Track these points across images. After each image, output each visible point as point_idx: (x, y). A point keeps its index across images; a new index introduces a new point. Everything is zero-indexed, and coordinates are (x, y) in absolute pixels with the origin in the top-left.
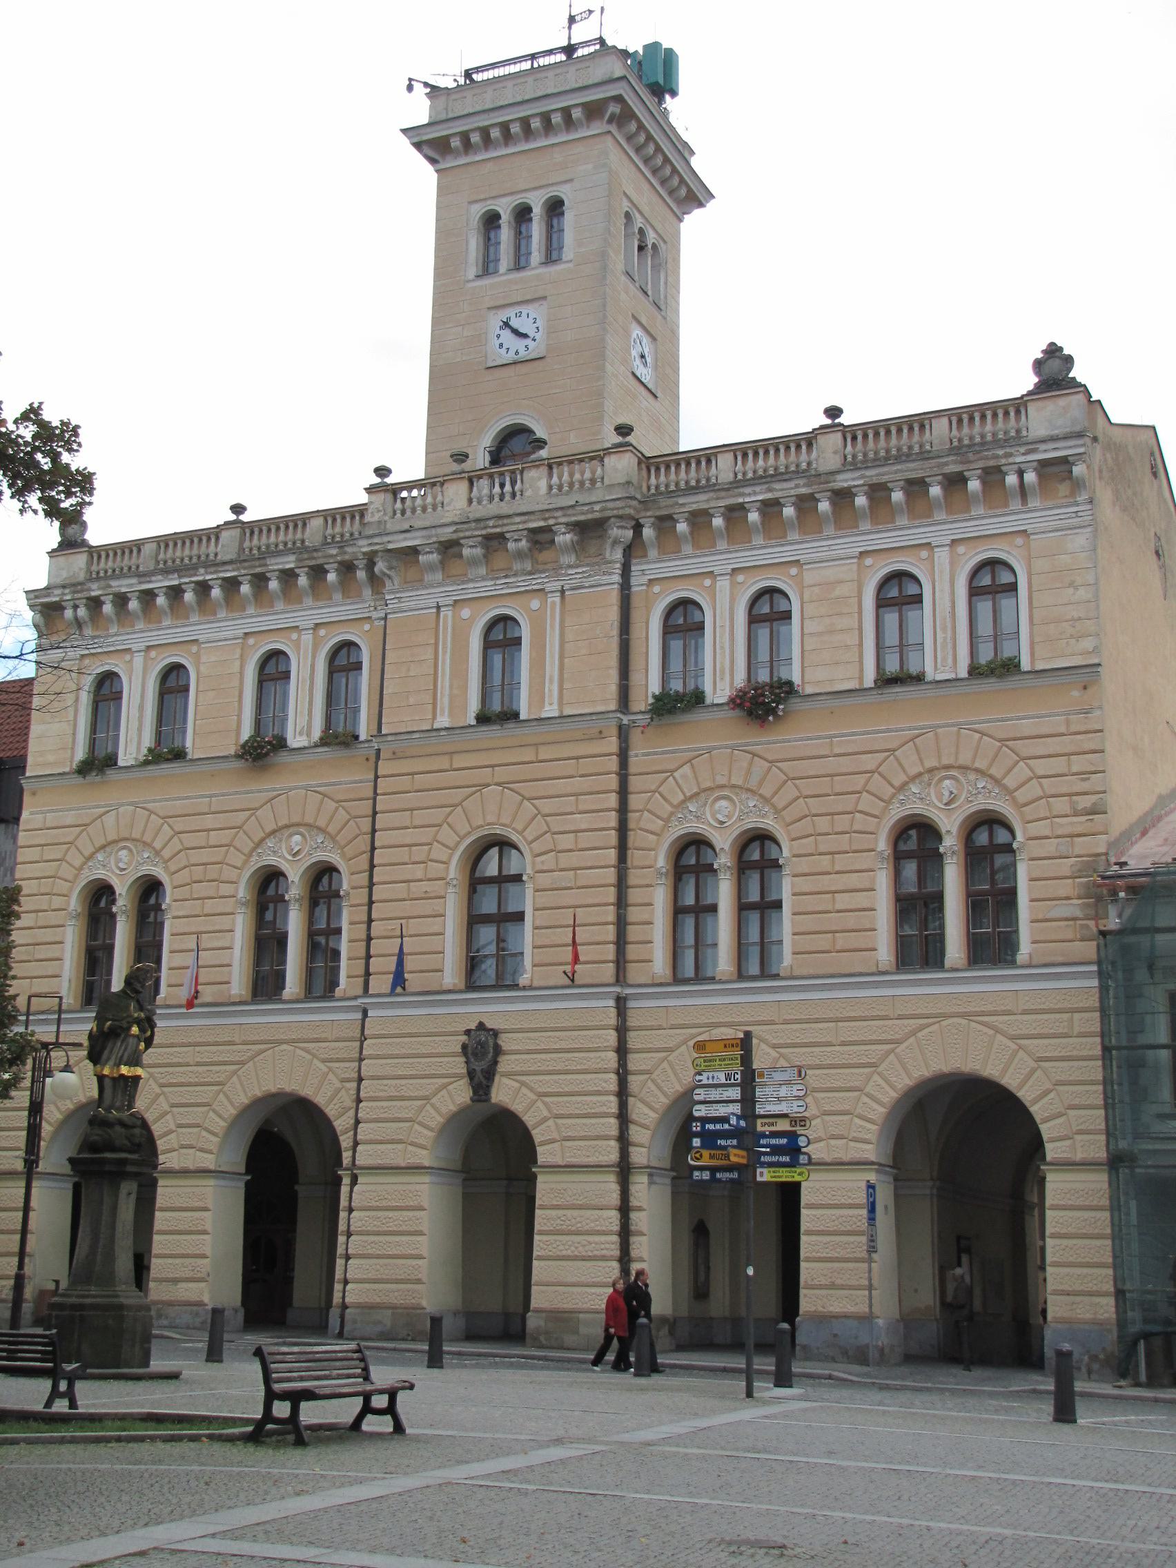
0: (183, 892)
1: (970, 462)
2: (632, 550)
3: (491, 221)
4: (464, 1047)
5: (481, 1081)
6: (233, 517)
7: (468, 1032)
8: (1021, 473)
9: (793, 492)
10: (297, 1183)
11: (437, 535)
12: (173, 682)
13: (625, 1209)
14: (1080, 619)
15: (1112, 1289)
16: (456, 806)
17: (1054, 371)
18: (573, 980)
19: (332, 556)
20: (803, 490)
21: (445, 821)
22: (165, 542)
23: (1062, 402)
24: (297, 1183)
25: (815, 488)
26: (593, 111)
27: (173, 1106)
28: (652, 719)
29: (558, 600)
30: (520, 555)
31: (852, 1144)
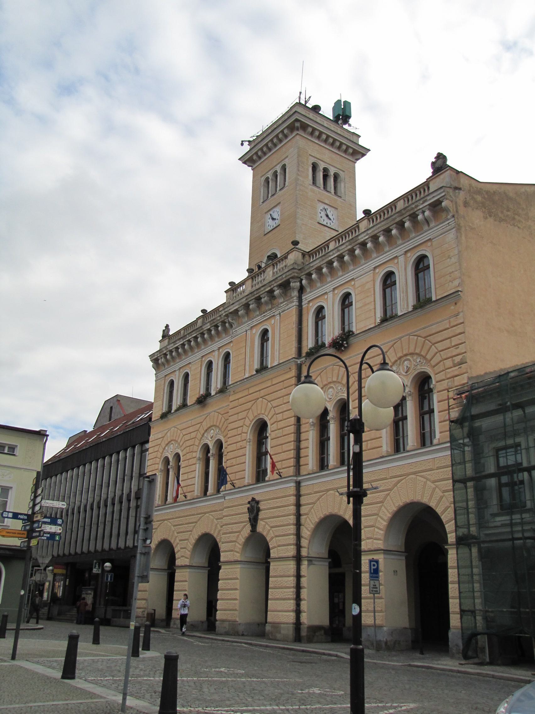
1: (404, 214)
2: (302, 290)
3: (267, 181)
5: (254, 521)
7: (249, 503)
9: (346, 249)
11: (242, 303)
13: (298, 576)
14: (453, 272)
15: (459, 611)
16: (249, 409)
17: (440, 164)
19: (219, 320)
20: (349, 247)
21: (247, 416)
22: (185, 328)
23: (442, 177)
25: (353, 245)
26: (292, 128)
28: (306, 359)
29: (278, 318)
30: (266, 303)
31: (375, 541)
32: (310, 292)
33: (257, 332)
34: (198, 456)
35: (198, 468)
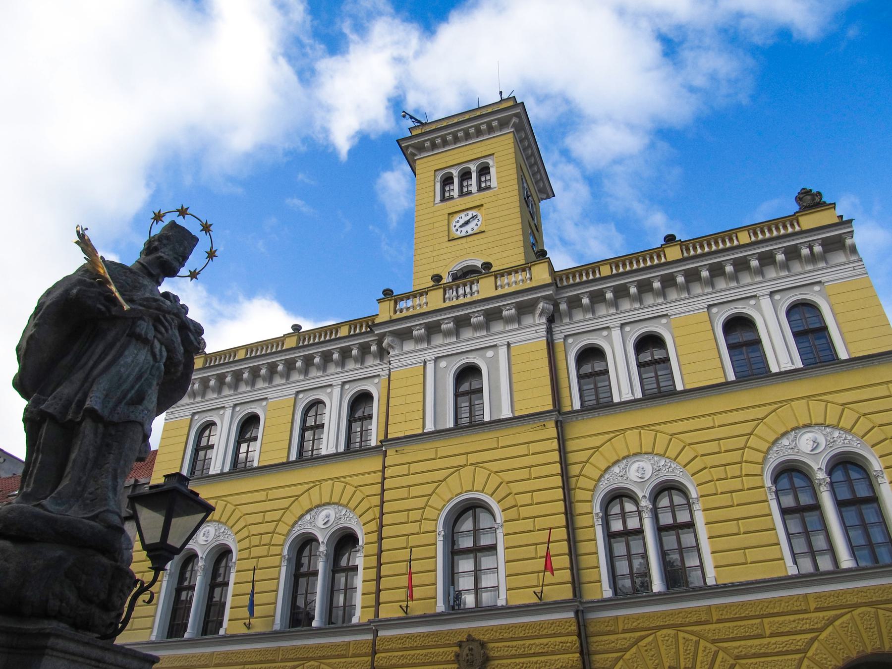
0: (245, 554)
4: (457, 656)
7: (460, 644)
8: (811, 248)
18: (406, 613)
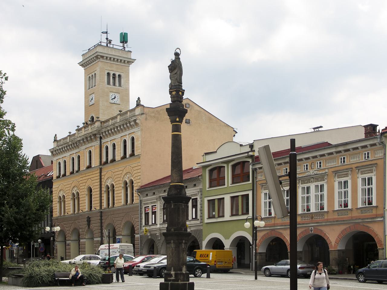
2: (101, 138)
6: (69, 134)
7: (87, 218)
10: (135, 233)
12: (341, 162)
24: (135, 233)
27: (136, 222)
32: (104, 139)
33: (88, 151)
34: (122, 186)
35: (123, 191)
